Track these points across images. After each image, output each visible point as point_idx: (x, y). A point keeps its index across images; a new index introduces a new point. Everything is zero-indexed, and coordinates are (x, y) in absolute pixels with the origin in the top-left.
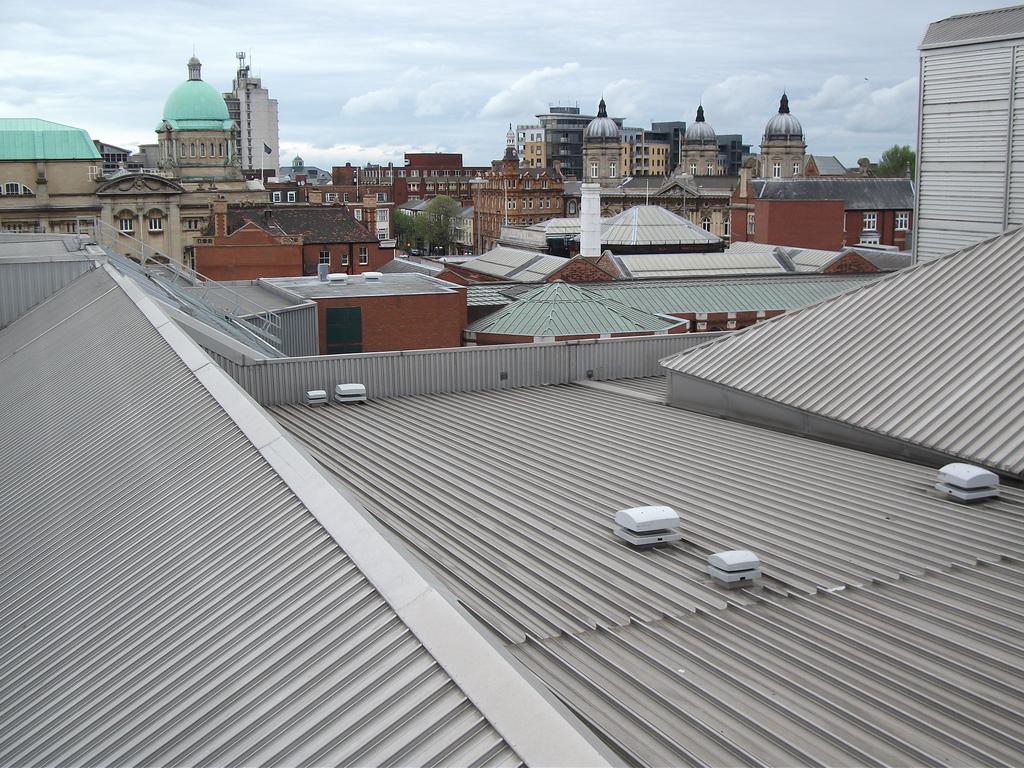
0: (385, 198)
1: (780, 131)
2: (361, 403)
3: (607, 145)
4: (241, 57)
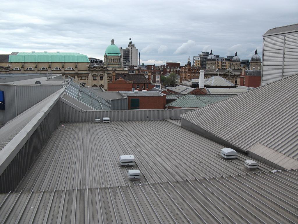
0: (159, 73)
1: (255, 58)
2: (109, 122)
3: (212, 61)
4: (130, 39)
